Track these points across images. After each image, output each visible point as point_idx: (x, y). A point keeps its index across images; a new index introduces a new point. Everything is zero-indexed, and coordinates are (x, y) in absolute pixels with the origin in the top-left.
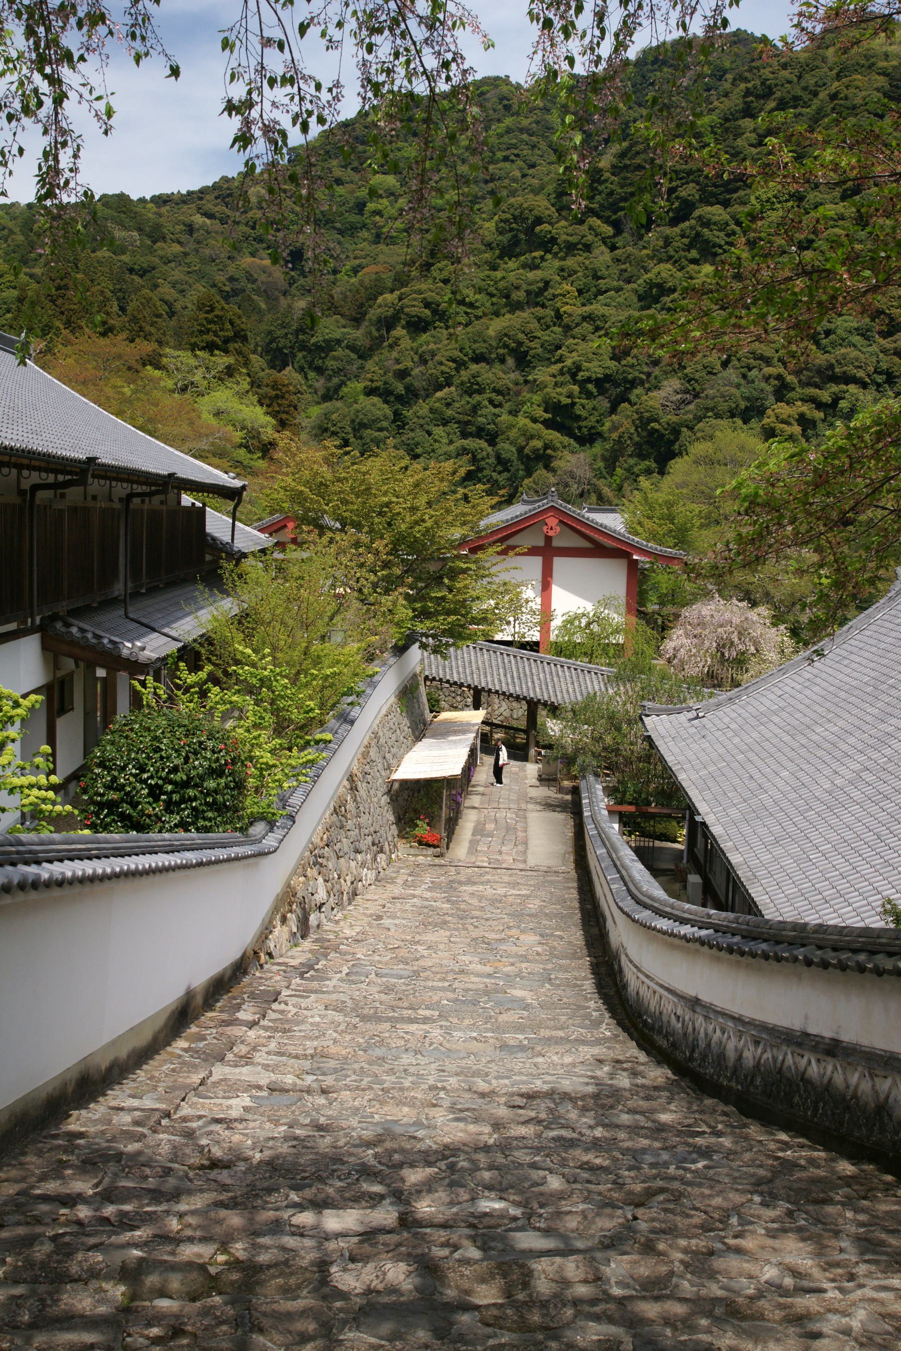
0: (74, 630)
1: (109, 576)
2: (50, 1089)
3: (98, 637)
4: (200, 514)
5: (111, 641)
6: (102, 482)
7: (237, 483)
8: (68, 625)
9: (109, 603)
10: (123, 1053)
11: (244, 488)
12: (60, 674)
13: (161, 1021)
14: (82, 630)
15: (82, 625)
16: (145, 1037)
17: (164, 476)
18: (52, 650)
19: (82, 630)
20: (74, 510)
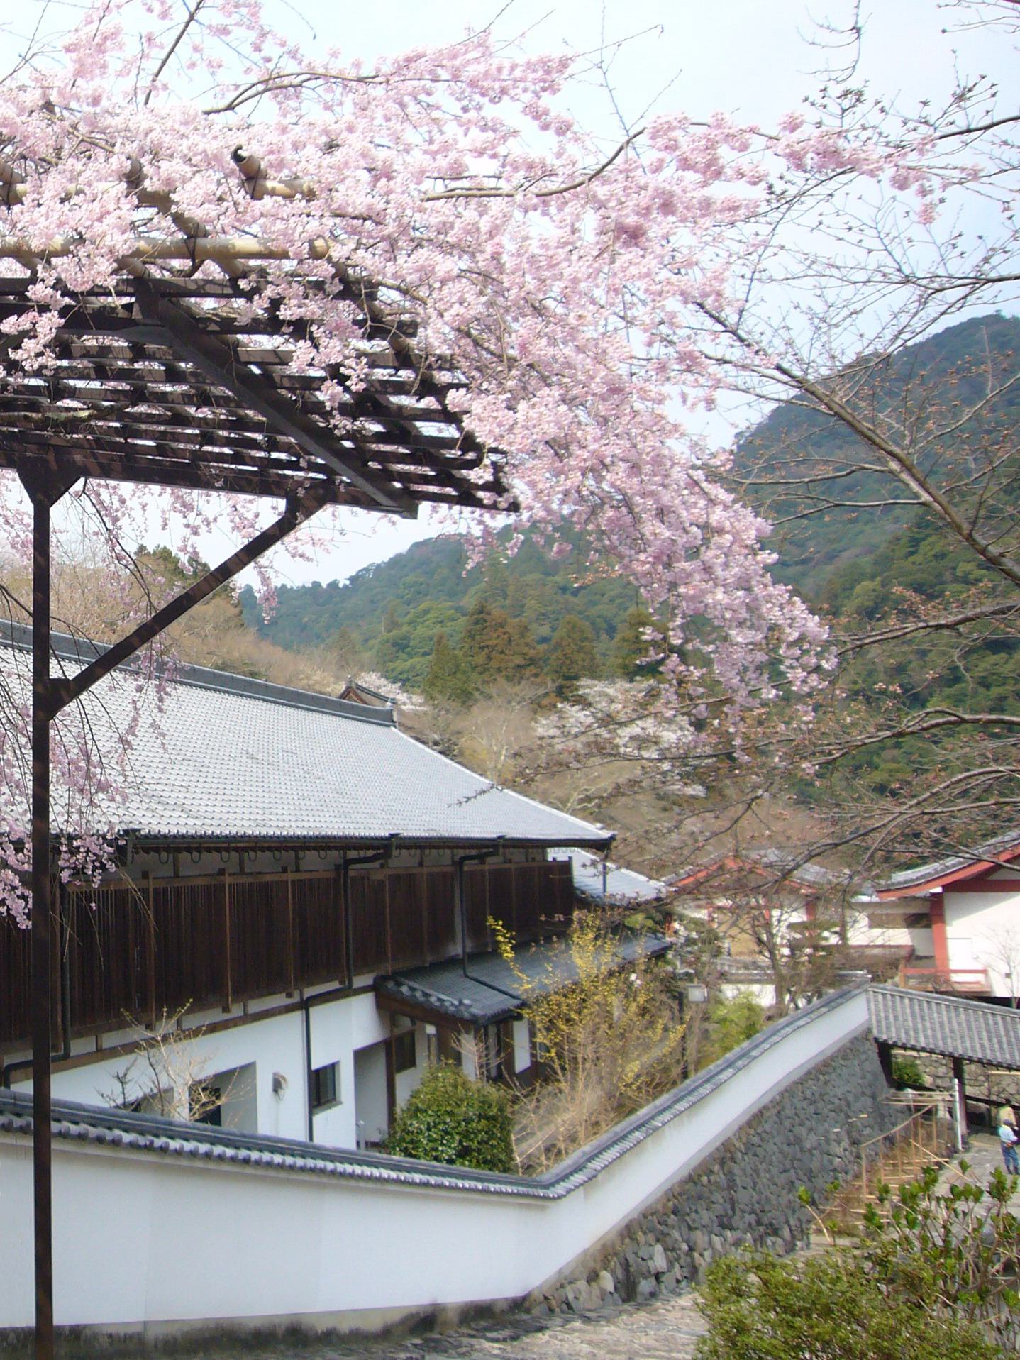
0: (404, 989)
1: (442, 933)
2: (258, 1323)
3: (426, 995)
4: (566, 867)
5: (439, 999)
6: (412, 851)
7: (605, 834)
8: (399, 984)
9: (453, 963)
10: (344, 1327)
11: (613, 838)
12: (397, 1031)
13: (396, 1317)
14: (412, 989)
15: (411, 984)
16: (374, 1325)
17: (493, 840)
18: (388, 1007)
19: (412, 989)
20: (396, 878)
